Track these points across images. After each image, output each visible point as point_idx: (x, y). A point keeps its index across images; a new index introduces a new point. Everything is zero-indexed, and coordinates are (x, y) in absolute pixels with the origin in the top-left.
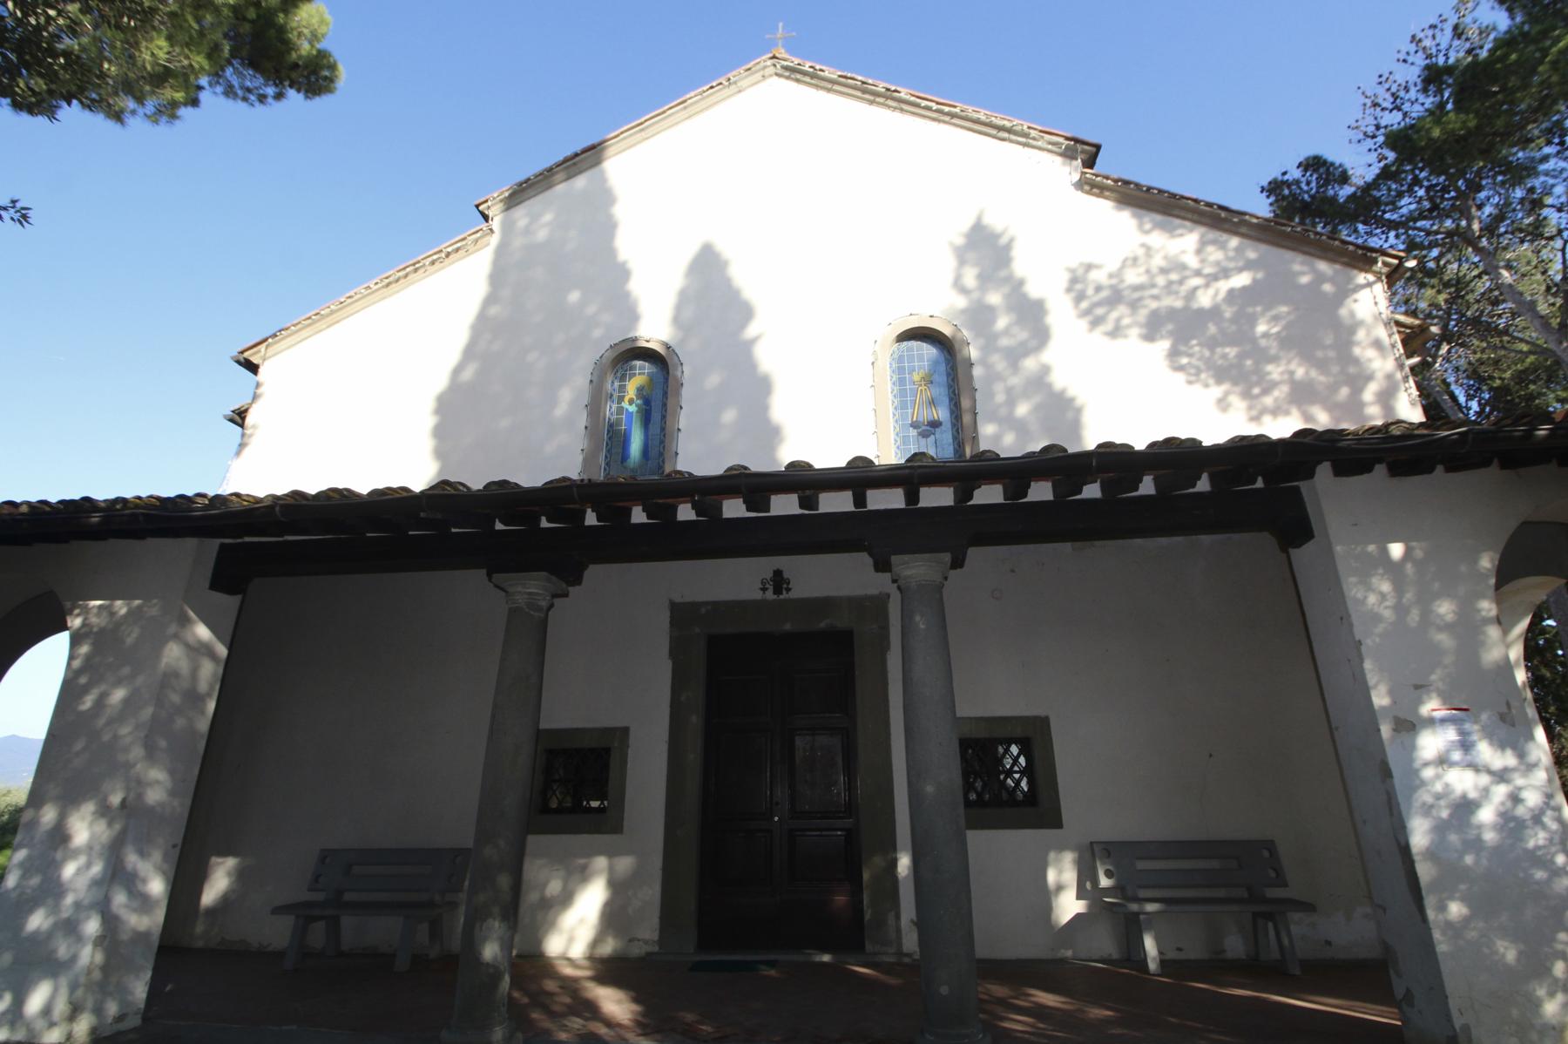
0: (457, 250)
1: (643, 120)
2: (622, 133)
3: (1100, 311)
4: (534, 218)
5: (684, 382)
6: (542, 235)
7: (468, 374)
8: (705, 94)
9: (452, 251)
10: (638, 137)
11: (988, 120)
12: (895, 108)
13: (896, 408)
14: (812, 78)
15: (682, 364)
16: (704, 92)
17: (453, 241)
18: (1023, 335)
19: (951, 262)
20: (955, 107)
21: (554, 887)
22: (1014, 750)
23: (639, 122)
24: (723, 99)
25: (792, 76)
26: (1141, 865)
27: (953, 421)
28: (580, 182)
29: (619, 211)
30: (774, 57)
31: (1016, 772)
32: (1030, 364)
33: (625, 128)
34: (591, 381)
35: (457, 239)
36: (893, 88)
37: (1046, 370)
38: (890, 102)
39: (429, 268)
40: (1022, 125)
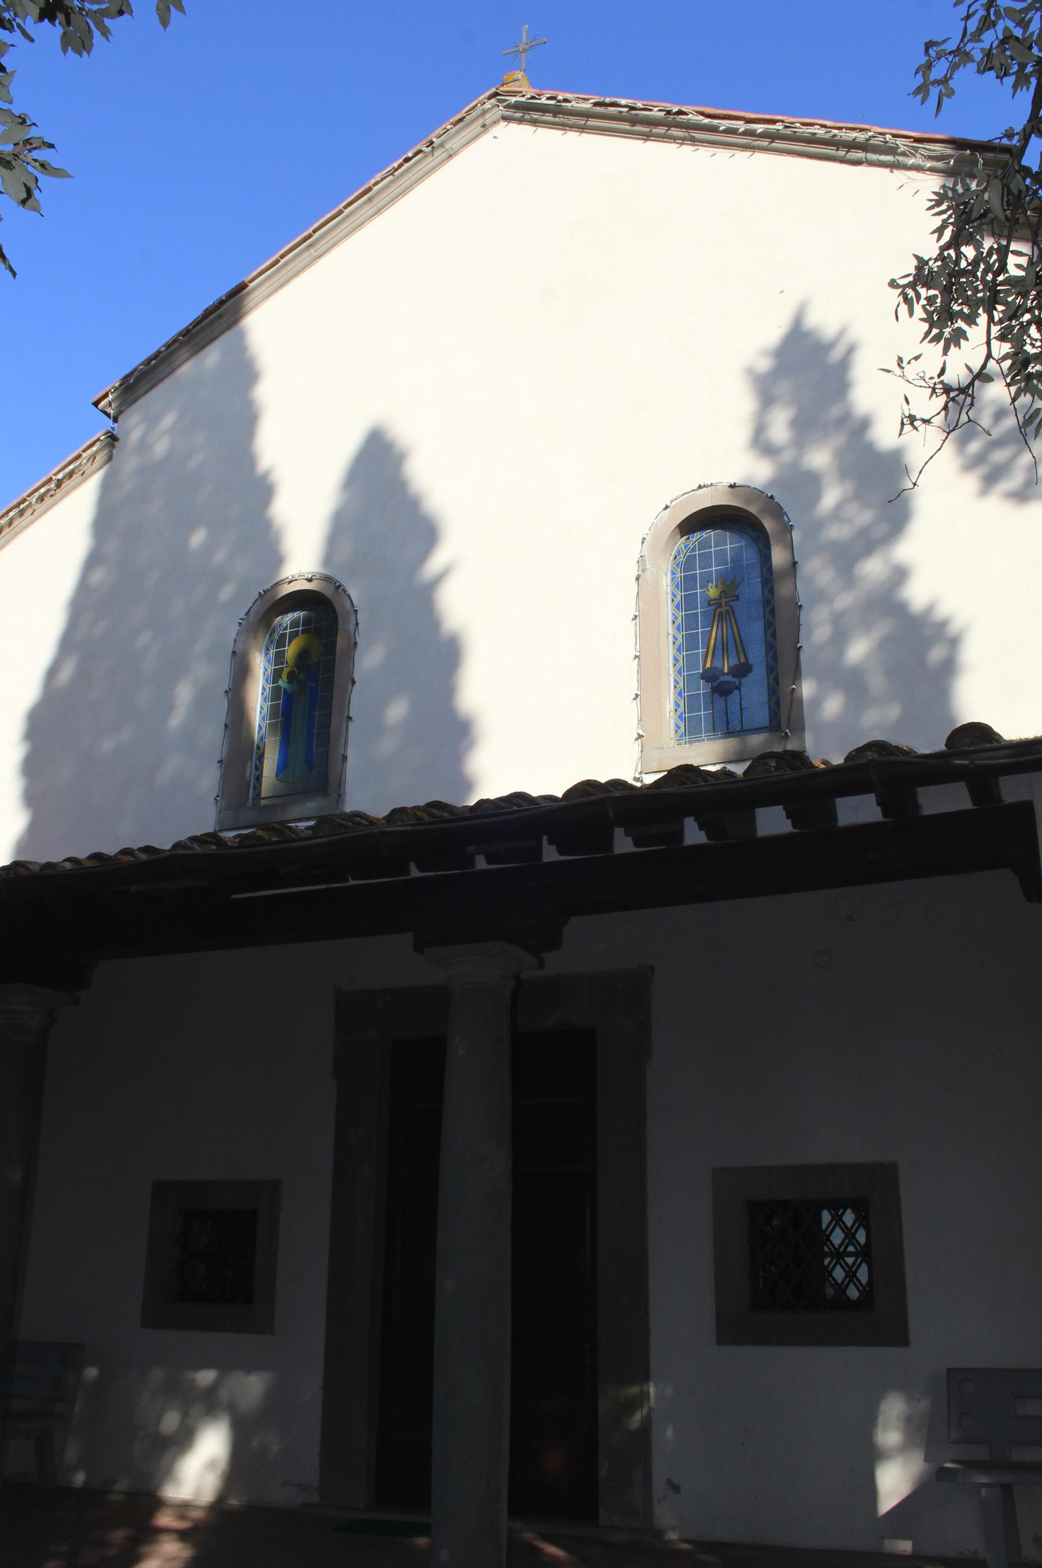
0: (71, 474)
1: (310, 231)
2: (282, 257)
3: (999, 456)
4: (152, 422)
5: (358, 640)
6: (160, 448)
7: (66, 674)
9: (64, 478)
10: (306, 257)
11: (827, 136)
13: (679, 650)
15: (356, 611)
16: (396, 170)
17: (64, 463)
18: (865, 517)
21: (171, 1421)
22: (849, 1218)
23: (305, 234)
25: (527, 117)
28: (212, 356)
31: (850, 1254)
35: (69, 458)
37: (900, 575)
38: (675, 132)
39: (37, 506)
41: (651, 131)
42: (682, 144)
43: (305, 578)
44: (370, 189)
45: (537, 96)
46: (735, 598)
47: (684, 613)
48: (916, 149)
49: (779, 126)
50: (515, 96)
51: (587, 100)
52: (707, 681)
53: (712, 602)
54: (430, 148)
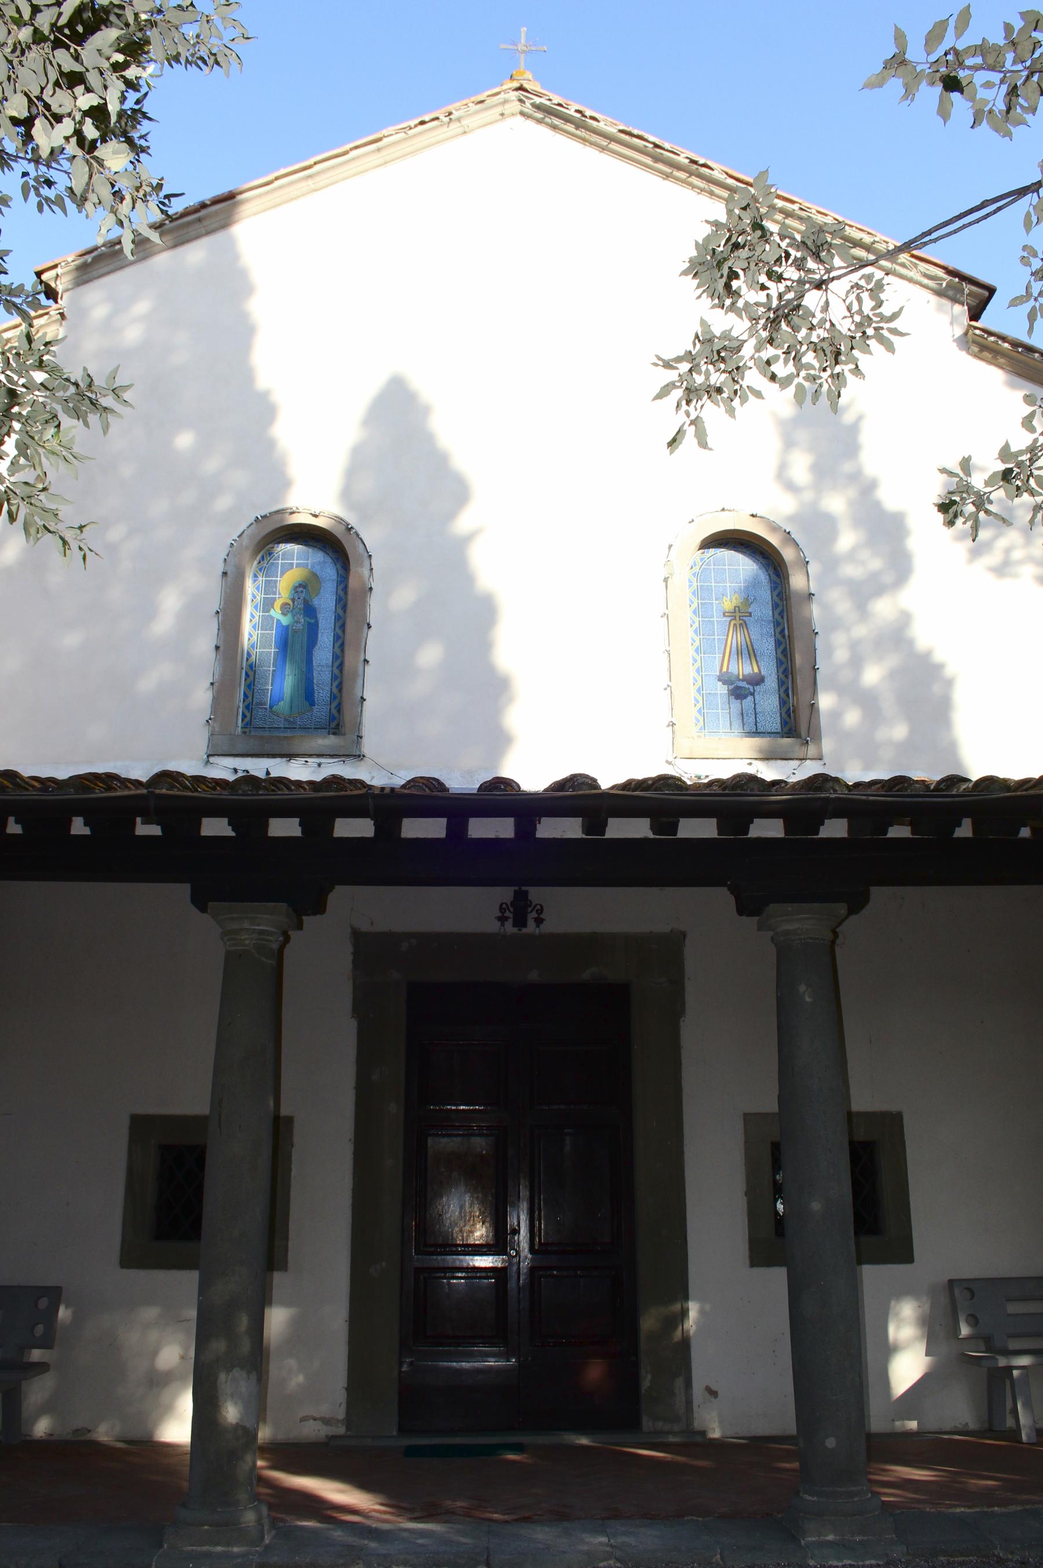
1: (311, 161)
6: (133, 334)
8: (411, 132)
10: (304, 186)
12: (702, 190)
14: (577, 128)
18: (876, 564)
19: (774, 442)
20: (793, 202)
24: (438, 142)
25: (547, 120)
26: (1012, 1308)
27: (781, 675)
29: (257, 307)
30: (521, 88)
32: (884, 608)
33: (283, 171)
34: (225, 574)
36: (701, 162)
37: (905, 619)
38: (694, 180)
40: (887, 243)
41: (672, 173)
42: (699, 193)
43: (310, 512)
44: (379, 140)
45: (564, 105)
46: (748, 614)
47: (261, 614)
48: (916, 266)
49: (796, 207)
50: (541, 97)
51: (616, 125)
52: (724, 684)
53: (726, 614)
54: (447, 118)
